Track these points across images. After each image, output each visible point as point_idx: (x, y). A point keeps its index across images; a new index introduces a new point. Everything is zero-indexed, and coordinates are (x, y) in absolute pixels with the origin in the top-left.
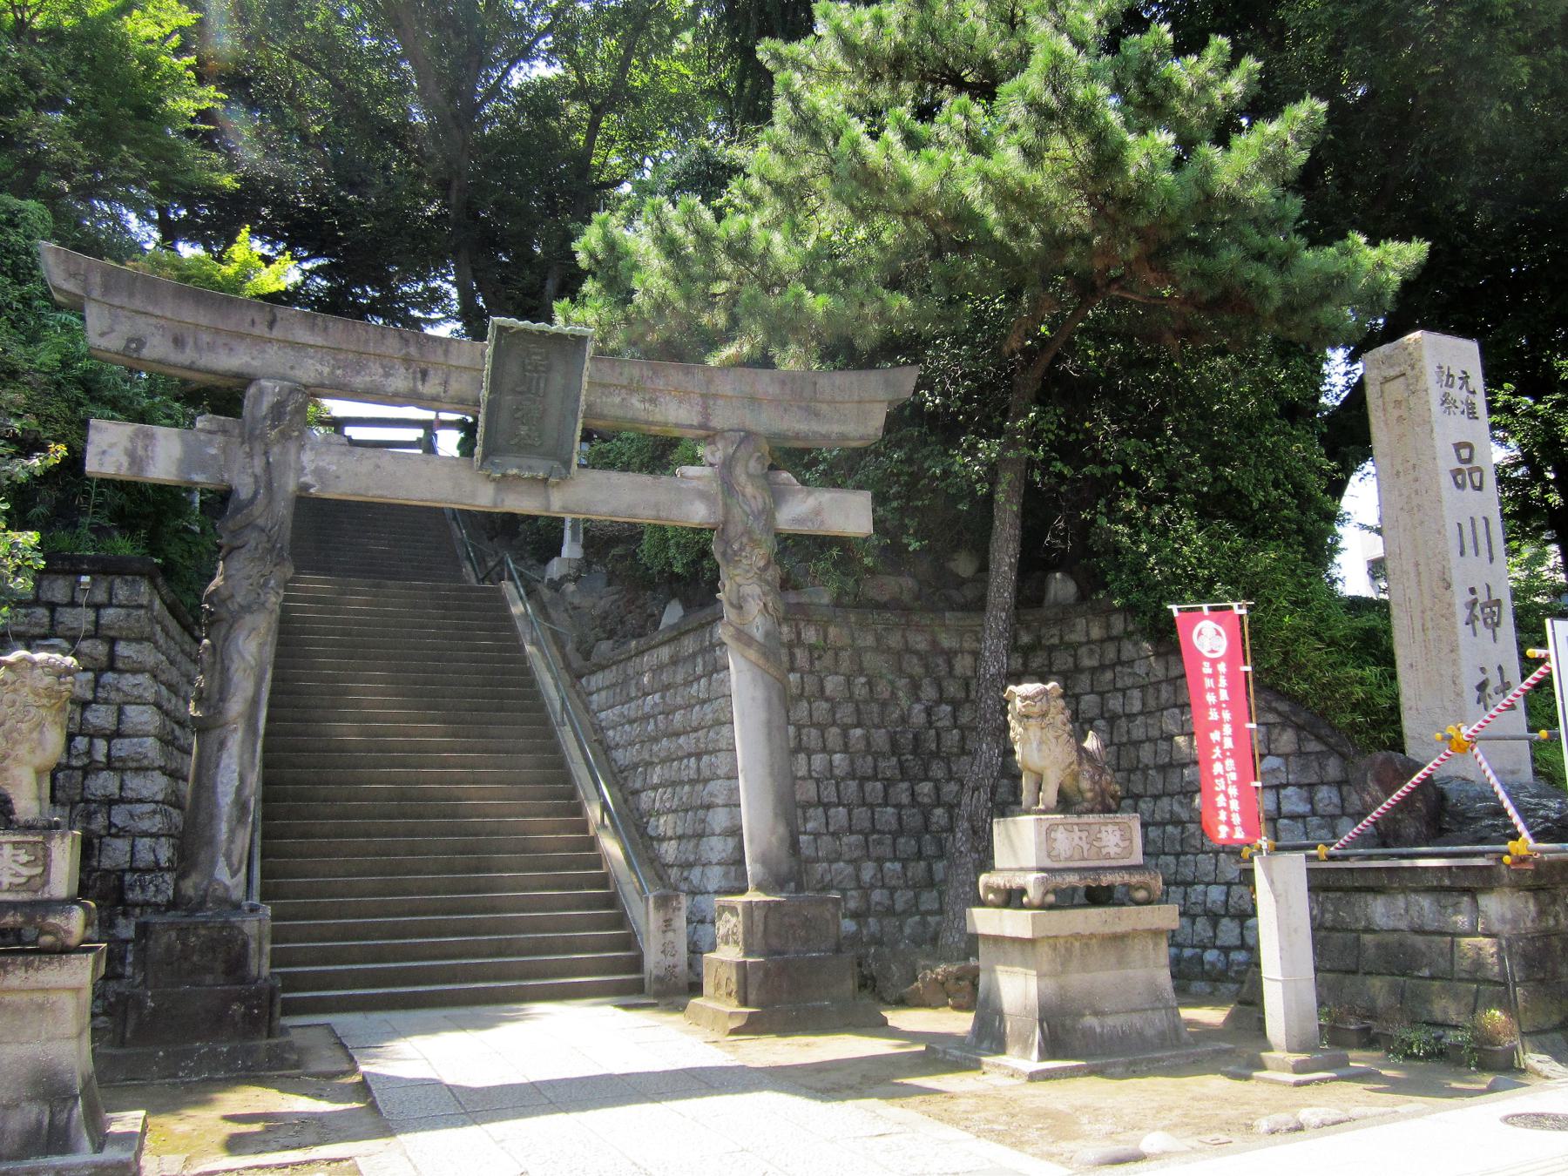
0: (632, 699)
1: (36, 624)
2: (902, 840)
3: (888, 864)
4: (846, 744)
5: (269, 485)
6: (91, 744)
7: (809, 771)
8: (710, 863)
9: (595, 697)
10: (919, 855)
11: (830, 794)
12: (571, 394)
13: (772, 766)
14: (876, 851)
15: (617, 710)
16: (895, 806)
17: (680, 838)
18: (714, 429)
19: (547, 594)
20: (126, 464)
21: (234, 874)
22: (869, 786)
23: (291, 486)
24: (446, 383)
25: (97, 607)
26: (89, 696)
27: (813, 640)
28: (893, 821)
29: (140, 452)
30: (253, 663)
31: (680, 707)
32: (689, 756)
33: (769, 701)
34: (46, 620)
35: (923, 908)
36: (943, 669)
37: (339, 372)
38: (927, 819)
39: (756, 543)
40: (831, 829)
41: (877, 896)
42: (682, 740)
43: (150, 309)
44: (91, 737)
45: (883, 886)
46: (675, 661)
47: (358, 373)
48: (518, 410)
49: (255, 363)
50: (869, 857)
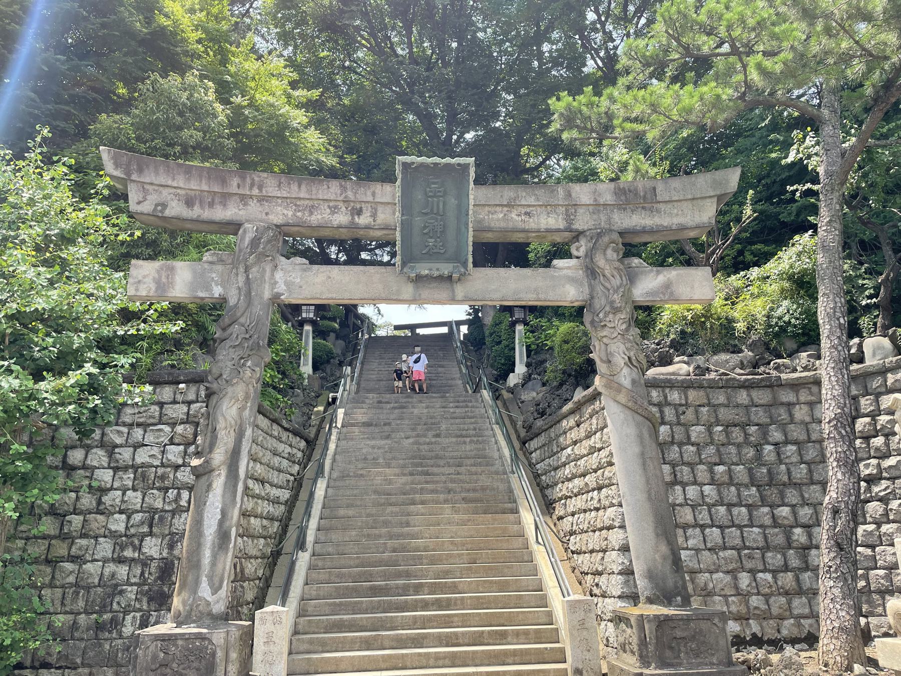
0: (555, 454)
1: (151, 417)
2: (769, 554)
3: (760, 575)
4: (712, 478)
5: (249, 294)
6: (179, 494)
7: (685, 499)
8: (613, 573)
9: (533, 455)
10: (786, 568)
11: (704, 517)
12: (462, 211)
13: (649, 492)
14: (749, 565)
15: (547, 461)
16: (760, 526)
17: (592, 552)
18: (577, 230)
19: (506, 395)
20: (154, 289)
21: (215, 590)
22: (735, 510)
23: (267, 295)
24: (374, 215)
25: (189, 403)
26: (180, 462)
28: (760, 538)
29: (164, 280)
32: (593, 490)
33: (640, 437)
34: (157, 414)
35: (796, 612)
36: (784, 416)
37: (299, 214)
38: (788, 538)
39: (616, 310)
41: (755, 601)
43: (170, 183)
44: (179, 489)
45: (758, 594)
48: (425, 227)
50: (743, 569)
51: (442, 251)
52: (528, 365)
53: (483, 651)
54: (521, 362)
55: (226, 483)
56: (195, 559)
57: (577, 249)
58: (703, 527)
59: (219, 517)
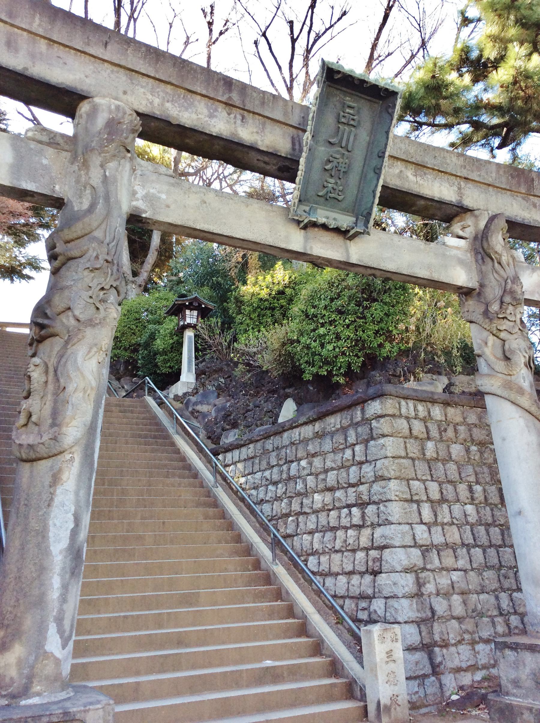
4: (473, 499)
15: (258, 475)
27: (439, 418)
30: (94, 384)
31: (333, 469)
40: (474, 566)
42: (339, 494)
46: (319, 436)
47: (187, 109)
49: (88, 81)
51: (340, 198)
52: (198, 376)
53: (186, 678)
54: (189, 370)
55: (80, 475)
56: (36, 592)
57: (463, 228)
58: (468, 547)
59: (72, 525)
